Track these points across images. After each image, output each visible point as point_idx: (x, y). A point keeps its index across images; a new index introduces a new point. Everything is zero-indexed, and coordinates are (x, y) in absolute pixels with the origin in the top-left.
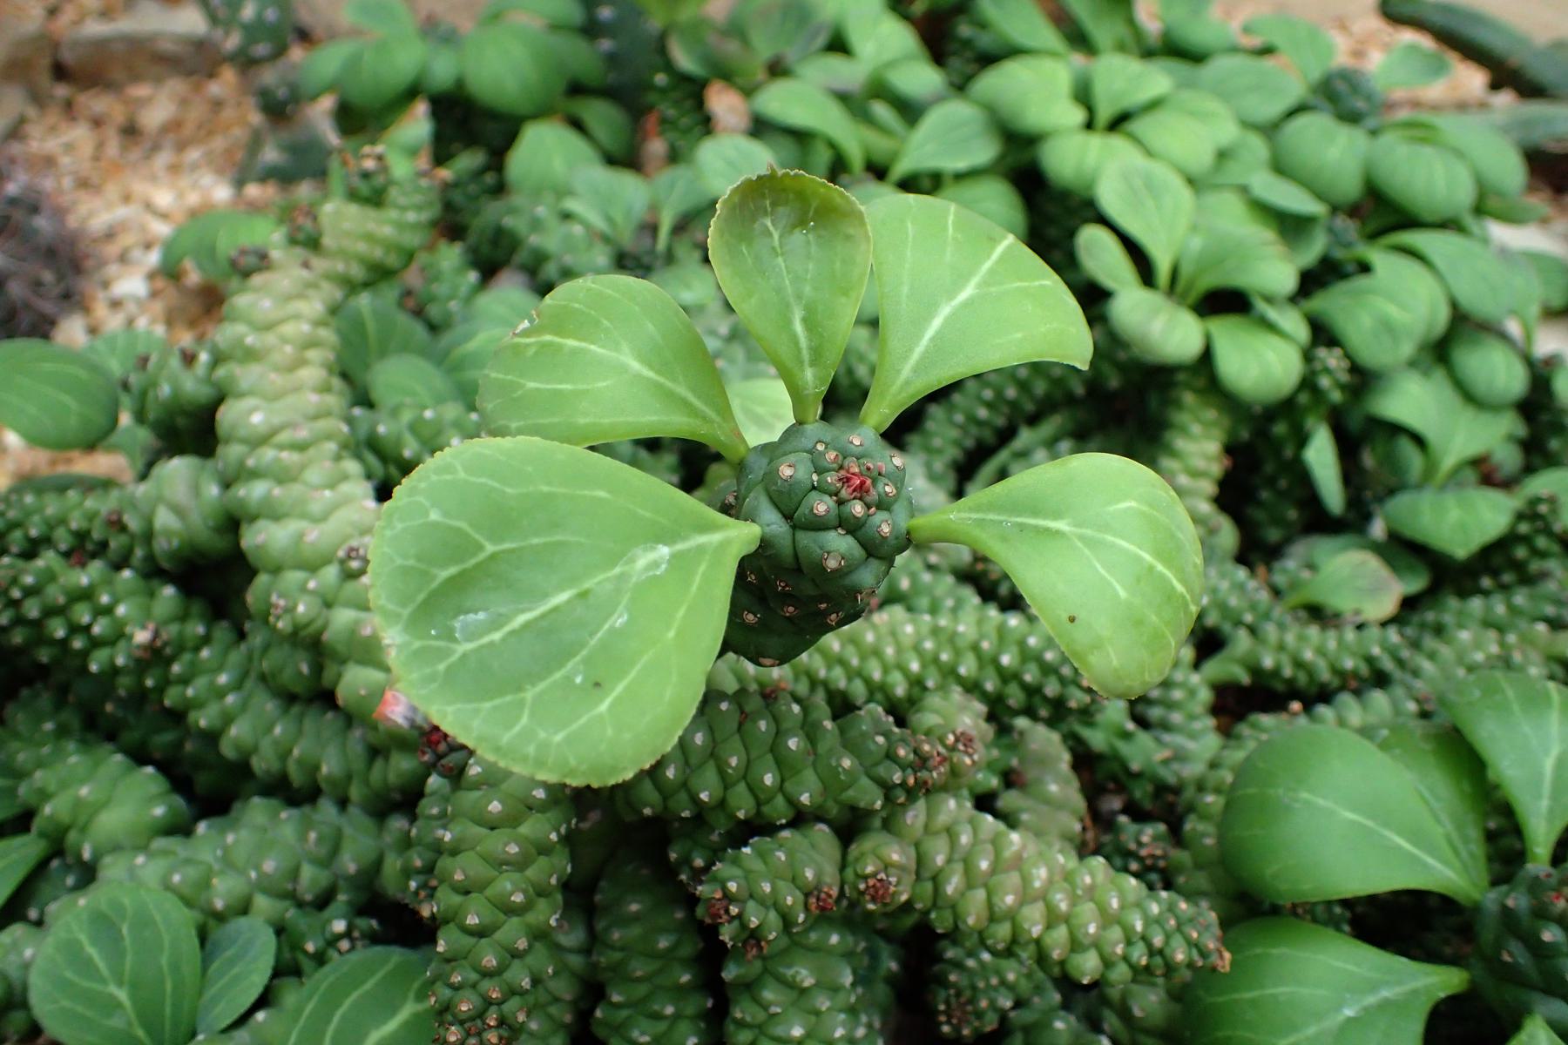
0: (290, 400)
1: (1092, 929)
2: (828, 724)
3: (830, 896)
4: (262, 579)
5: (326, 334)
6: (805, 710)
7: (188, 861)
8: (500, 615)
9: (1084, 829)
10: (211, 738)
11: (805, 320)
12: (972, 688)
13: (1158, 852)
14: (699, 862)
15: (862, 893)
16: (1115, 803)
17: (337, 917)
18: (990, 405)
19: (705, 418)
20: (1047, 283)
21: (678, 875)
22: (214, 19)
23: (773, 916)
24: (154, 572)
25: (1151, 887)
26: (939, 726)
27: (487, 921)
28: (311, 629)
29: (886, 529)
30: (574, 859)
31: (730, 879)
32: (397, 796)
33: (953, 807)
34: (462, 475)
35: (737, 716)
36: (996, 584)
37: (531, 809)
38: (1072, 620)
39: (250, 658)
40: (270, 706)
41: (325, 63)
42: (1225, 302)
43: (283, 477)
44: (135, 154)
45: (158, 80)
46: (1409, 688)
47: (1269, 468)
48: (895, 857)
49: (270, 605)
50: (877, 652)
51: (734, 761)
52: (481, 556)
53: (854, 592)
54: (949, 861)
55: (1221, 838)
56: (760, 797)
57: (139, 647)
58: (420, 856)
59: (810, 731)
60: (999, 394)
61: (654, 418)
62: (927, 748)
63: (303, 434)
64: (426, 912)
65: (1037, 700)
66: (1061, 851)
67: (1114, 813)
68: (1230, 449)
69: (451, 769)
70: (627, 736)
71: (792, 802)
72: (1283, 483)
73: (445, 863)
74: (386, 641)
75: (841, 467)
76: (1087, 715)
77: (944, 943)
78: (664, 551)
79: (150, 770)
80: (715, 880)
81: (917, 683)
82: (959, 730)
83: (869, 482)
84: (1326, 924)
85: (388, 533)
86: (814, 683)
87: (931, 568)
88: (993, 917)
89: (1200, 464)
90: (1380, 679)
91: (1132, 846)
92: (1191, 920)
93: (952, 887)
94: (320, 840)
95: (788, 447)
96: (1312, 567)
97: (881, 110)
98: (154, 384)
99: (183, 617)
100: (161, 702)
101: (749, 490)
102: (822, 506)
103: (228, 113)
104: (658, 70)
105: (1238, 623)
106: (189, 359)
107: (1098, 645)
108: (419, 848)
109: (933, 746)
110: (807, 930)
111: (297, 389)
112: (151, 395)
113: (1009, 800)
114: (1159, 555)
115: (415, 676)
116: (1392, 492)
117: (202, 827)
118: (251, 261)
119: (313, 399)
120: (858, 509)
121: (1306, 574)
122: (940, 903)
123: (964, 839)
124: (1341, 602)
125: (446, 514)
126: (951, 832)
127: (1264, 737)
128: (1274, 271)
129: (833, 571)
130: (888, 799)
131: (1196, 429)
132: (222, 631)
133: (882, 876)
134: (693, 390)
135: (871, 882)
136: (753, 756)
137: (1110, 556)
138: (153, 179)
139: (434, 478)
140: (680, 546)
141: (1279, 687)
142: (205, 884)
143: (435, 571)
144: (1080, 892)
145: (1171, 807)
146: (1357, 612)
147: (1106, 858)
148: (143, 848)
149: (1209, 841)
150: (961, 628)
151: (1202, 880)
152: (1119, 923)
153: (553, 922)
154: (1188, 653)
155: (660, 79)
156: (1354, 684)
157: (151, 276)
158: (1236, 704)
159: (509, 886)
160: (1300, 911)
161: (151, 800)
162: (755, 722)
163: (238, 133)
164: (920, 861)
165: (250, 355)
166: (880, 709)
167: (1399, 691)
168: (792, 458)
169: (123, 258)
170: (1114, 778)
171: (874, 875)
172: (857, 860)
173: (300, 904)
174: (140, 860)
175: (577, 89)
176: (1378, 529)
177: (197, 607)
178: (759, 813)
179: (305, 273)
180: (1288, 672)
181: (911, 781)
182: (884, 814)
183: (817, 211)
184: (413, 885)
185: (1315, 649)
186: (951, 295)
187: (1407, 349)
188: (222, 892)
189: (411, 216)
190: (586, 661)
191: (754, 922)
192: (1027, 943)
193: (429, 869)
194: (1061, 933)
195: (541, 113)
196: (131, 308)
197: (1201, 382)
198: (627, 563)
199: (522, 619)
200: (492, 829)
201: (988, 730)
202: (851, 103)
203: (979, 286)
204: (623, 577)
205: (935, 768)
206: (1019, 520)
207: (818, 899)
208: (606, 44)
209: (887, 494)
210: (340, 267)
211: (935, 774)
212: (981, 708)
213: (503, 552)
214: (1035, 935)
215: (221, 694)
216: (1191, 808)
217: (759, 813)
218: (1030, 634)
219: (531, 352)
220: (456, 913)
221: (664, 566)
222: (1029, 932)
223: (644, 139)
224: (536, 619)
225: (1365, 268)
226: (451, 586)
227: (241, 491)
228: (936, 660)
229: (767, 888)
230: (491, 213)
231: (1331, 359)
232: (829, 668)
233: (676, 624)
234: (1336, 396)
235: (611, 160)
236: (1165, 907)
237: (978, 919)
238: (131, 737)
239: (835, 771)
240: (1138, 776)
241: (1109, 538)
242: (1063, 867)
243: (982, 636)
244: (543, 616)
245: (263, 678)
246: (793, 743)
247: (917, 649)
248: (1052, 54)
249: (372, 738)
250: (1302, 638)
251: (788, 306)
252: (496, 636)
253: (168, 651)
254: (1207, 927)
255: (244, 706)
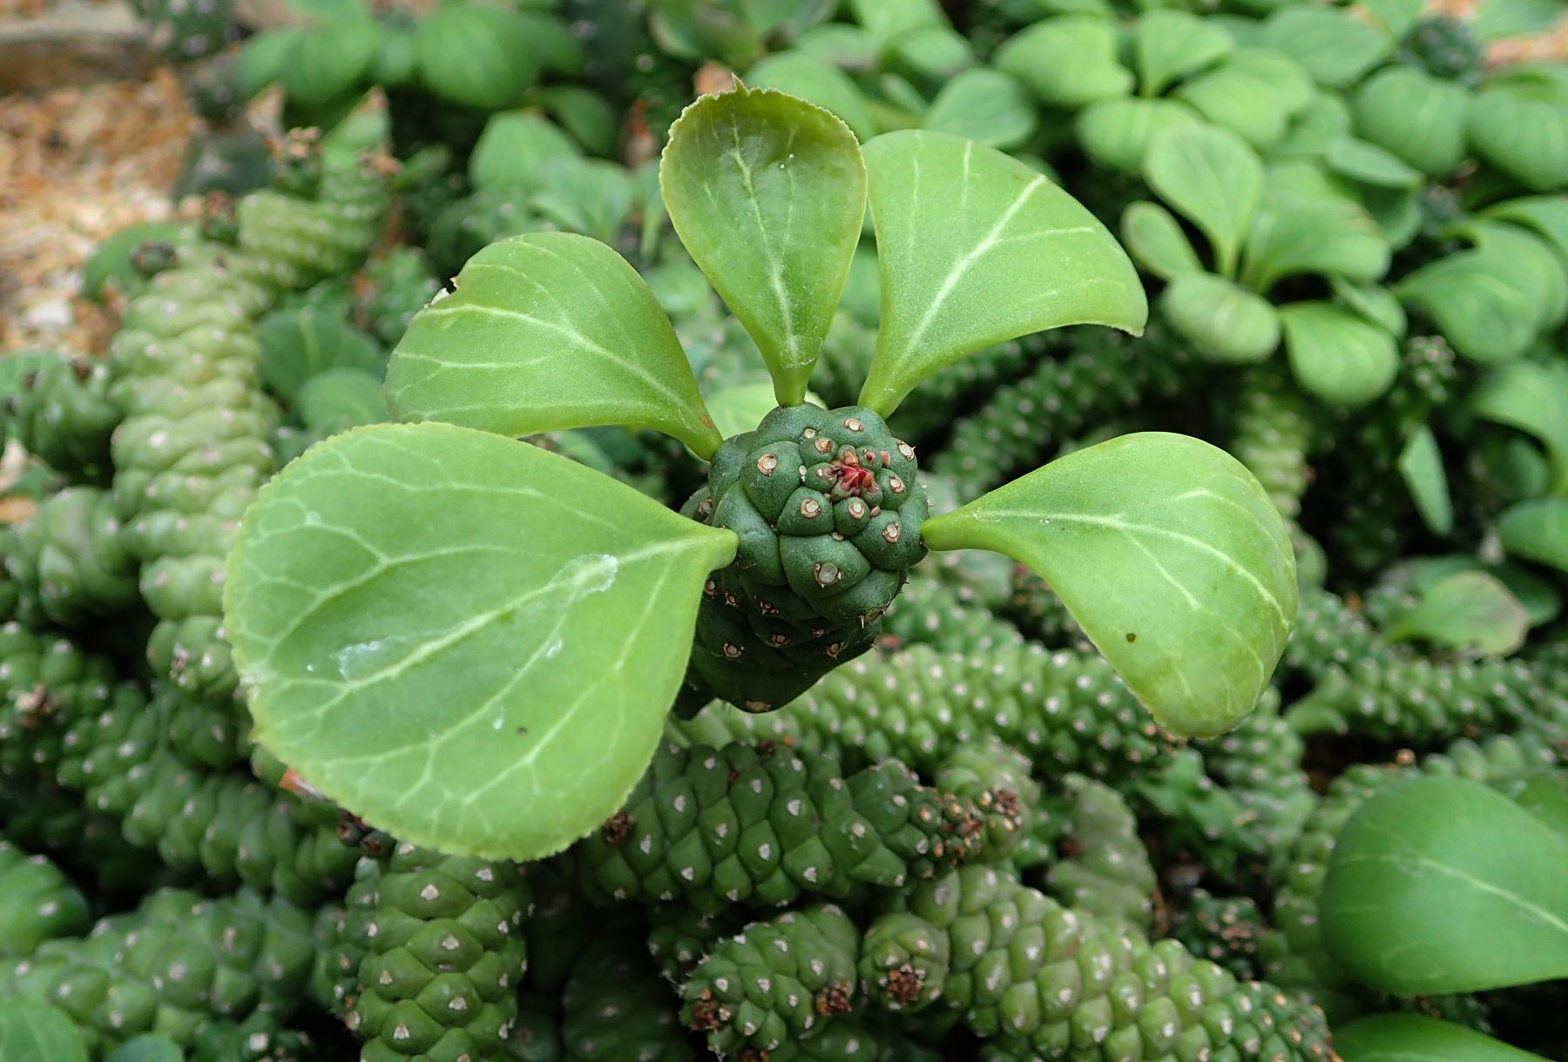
0: (201, 418)
1: (1169, 1031)
2: (837, 783)
3: (842, 994)
4: (164, 630)
5: (244, 342)
6: (809, 765)
7: (81, 969)
8: (399, 644)
9: (1154, 907)
10: (115, 819)
11: (784, 276)
12: (1013, 738)
13: (1246, 934)
14: (685, 955)
15: (881, 989)
16: (1189, 876)
17: (257, 1032)
18: (1028, 419)
19: (665, 402)
20: (1089, 230)
21: (660, 970)
22: (140, 10)
23: (773, 1022)
24: (44, 626)
25: (1239, 978)
26: (972, 783)
27: (418, 1034)
28: (220, 686)
29: (893, 533)
30: (531, 954)
31: (720, 975)
32: (329, 883)
33: (991, 882)
34: (349, 469)
35: (725, 775)
36: (1039, 620)
37: (475, 894)
38: (1131, 638)
39: (157, 723)
40: (181, 779)
41: (264, 56)
42: (1303, 288)
43: (192, 506)
44: (62, 165)
45: (85, 86)
46: (1541, 733)
47: (1359, 480)
48: (923, 944)
49: (172, 658)
50: (899, 700)
51: (722, 831)
52: (375, 571)
53: (856, 612)
54: (990, 948)
55: (1323, 917)
56: (756, 874)
57: (22, 714)
58: (348, 956)
59: (815, 793)
60: (1039, 405)
61: (602, 402)
62: (957, 809)
63: (214, 457)
64: (354, 1022)
65: (1091, 753)
66: (1128, 934)
67: (1189, 889)
68: (1314, 460)
69: (378, 847)
70: (560, 795)
71: (794, 879)
72: (1377, 498)
73: (371, 963)
74: (246, 680)
75: (835, 458)
76: (1151, 767)
77: (990, 1048)
78: (611, 562)
79: (40, 860)
80: (701, 976)
81: (948, 736)
82: (997, 788)
83: (870, 474)
84: (1456, 1020)
85: (251, 543)
86: (826, 738)
87: (964, 604)
88: (1046, 1017)
89: (1276, 476)
90: (1506, 724)
91: (1213, 927)
92: (1292, 1018)
93: (994, 978)
94: (238, 938)
95: (769, 436)
96: (1415, 593)
97: (896, 87)
98: (41, 405)
99: (79, 678)
100: (54, 777)
101: (722, 492)
102: (812, 505)
103: (167, 122)
104: (640, 52)
105: (1329, 660)
106: (82, 375)
107: (1165, 669)
108: (349, 946)
109: (965, 808)
110: (817, 1038)
111: (209, 405)
112: (39, 420)
113: (1062, 873)
114: (1240, 554)
115: (283, 724)
116: (1507, 504)
117: (102, 927)
118: (153, 259)
119: (226, 416)
120: (857, 508)
121: (1408, 603)
122: (980, 1000)
123: (1008, 921)
124: (1456, 634)
125: (326, 518)
126: (990, 913)
127: (1370, 793)
128: (1361, 249)
129: (828, 586)
130: (912, 873)
131: (1271, 436)
132: (127, 694)
133: (907, 968)
134: (650, 369)
135: (894, 976)
136: (746, 821)
137: (1174, 556)
138: (79, 195)
139: (313, 474)
140: (630, 557)
141: (1382, 735)
142: (99, 995)
143: (312, 589)
144: (1151, 985)
145: (1258, 880)
146: (1474, 645)
147: (1181, 941)
148: (28, 954)
149: (1308, 920)
150: (999, 669)
151: (1300, 968)
152: (1202, 1022)
153: (503, 1033)
154: (1270, 698)
155: (645, 62)
156: (1475, 730)
157: (74, 301)
158: (1328, 758)
159: (446, 991)
160: (1425, 1005)
161: (41, 896)
162: (747, 782)
163: (177, 145)
164: (955, 948)
165: (154, 367)
166: (901, 766)
167: (1530, 738)
168: (774, 448)
169: (44, 282)
170: (1188, 846)
171: (897, 967)
172: (876, 948)
173: (216, 1017)
174: (23, 968)
175: (551, 78)
176: (1492, 549)
177: (96, 666)
178: (754, 894)
179: (218, 274)
180: (1392, 716)
181: (939, 851)
182: (907, 891)
183: (796, 140)
184: (339, 990)
185: (1424, 689)
186: (968, 247)
187: (1522, 336)
188: (121, 1004)
189: (351, 212)
190: (508, 701)
191: (750, 1028)
192: (1089, 1049)
193: (354, 972)
194: (1130, 1036)
195: (512, 104)
196: (50, 338)
197: (1275, 381)
198: (563, 578)
199: (427, 649)
200: (428, 919)
201: (1033, 789)
202: (862, 80)
203: (1003, 235)
204: (556, 595)
205: (969, 834)
206: (1060, 516)
207: (829, 998)
208: (584, 28)
209: (893, 490)
210: (262, 266)
211: (968, 842)
212: (1022, 761)
213: (403, 565)
214: (1098, 1039)
215: (124, 766)
216: (1283, 881)
217: (754, 894)
218: (1081, 674)
219: (447, 325)
220: (382, 1026)
221: (610, 581)
222: (1091, 1035)
223: (631, 134)
224: (444, 650)
225: (1467, 244)
226: (336, 605)
227: (140, 526)
228: (969, 708)
229: (765, 985)
230: (454, 218)
231: (1431, 350)
232: (843, 719)
233: (624, 654)
234: (1438, 394)
235: (590, 153)
236: (1258, 1002)
237: (1027, 1018)
238: (20, 823)
239: (845, 839)
240: (1215, 843)
241: (1174, 535)
242: (1130, 953)
243: (1024, 678)
244: (454, 645)
245: (172, 747)
246: (793, 807)
247: (947, 695)
248: (1092, 15)
249: (302, 815)
250: (1408, 677)
251: (763, 258)
252: (393, 672)
253: (60, 718)
254: (1312, 1027)
255: (151, 782)
